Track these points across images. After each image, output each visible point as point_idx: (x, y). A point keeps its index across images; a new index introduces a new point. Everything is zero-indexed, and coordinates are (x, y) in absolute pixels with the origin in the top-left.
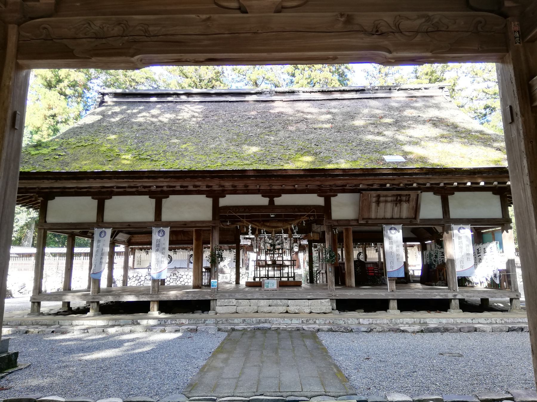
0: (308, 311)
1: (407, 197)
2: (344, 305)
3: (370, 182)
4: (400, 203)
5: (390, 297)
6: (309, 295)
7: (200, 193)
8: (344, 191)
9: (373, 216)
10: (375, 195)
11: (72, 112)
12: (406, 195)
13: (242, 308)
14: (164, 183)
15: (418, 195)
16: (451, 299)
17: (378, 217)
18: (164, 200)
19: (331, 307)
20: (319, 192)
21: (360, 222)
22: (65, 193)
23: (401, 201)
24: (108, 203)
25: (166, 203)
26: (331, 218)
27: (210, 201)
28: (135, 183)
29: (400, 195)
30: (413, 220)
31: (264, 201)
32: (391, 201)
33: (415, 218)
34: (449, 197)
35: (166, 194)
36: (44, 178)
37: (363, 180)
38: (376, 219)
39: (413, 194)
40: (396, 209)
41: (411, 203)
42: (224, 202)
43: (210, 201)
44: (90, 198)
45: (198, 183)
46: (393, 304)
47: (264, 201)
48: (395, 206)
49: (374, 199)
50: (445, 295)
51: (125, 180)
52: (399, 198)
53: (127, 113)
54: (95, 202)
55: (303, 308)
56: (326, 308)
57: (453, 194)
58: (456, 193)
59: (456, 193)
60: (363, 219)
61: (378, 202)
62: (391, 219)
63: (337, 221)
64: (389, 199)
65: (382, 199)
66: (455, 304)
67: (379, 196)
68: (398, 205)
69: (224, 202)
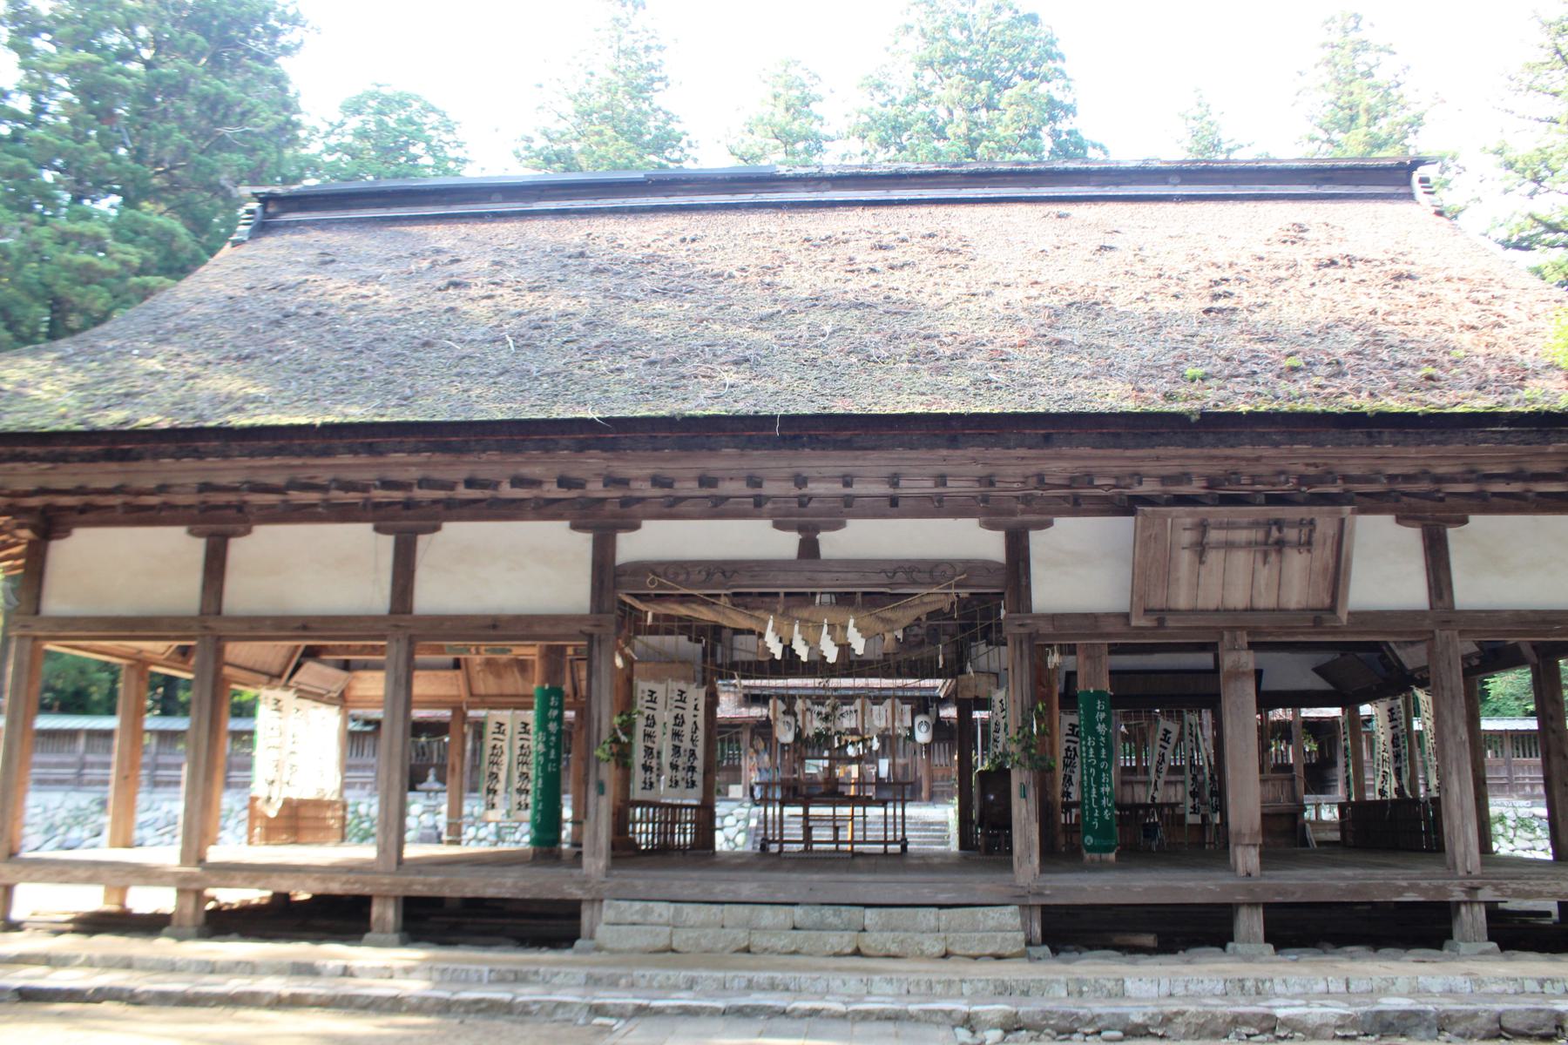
0: (938, 949)
1: (1305, 531)
2: (1067, 931)
3: (1172, 468)
4: (1280, 552)
5: (1239, 898)
6: (943, 891)
7: (545, 510)
8: (1077, 506)
9: (1182, 601)
10: (1188, 521)
12: (1301, 523)
13: (693, 934)
15: (1342, 521)
16: (1458, 904)
17: (1201, 604)
18: (423, 541)
19: (1021, 936)
20: (985, 508)
21: (1134, 623)
22: (95, 513)
23: (1280, 545)
24: (238, 549)
26: (1029, 609)
28: (312, 472)
29: (1279, 524)
30: (1326, 616)
31: (786, 544)
32: (1249, 545)
33: (1332, 609)
34: (1452, 533)
35: (51, 524)
37: (1143, 459)
38: (1193, 611)
39: (1324, 520)
40: (1264, 573)
41: (1317, 552)
42: (632, 546)
44: (366, 529)
45: (669, 469)
46: (1250, 923)
47: (786, 544)
48: (1259, 564)
49: (1187, 537)
50: (1438, 889)
51: (277, 460)
52: (1275, 533)
54: (198, 546)
55: (918, 937)
56: (1005, 940)
57: (1465, 521)
58: (1472, 518)
59: (1472, 518)
60: (1147, 611)
61: (1201, 549)
62: (1246, 610)
63: (1054, 618)
64: (1242, 536)
65: (1214, 535)
66: (1473, 919)
67: (1203, 527)
68: (1273, 557)
69: (632, 546)
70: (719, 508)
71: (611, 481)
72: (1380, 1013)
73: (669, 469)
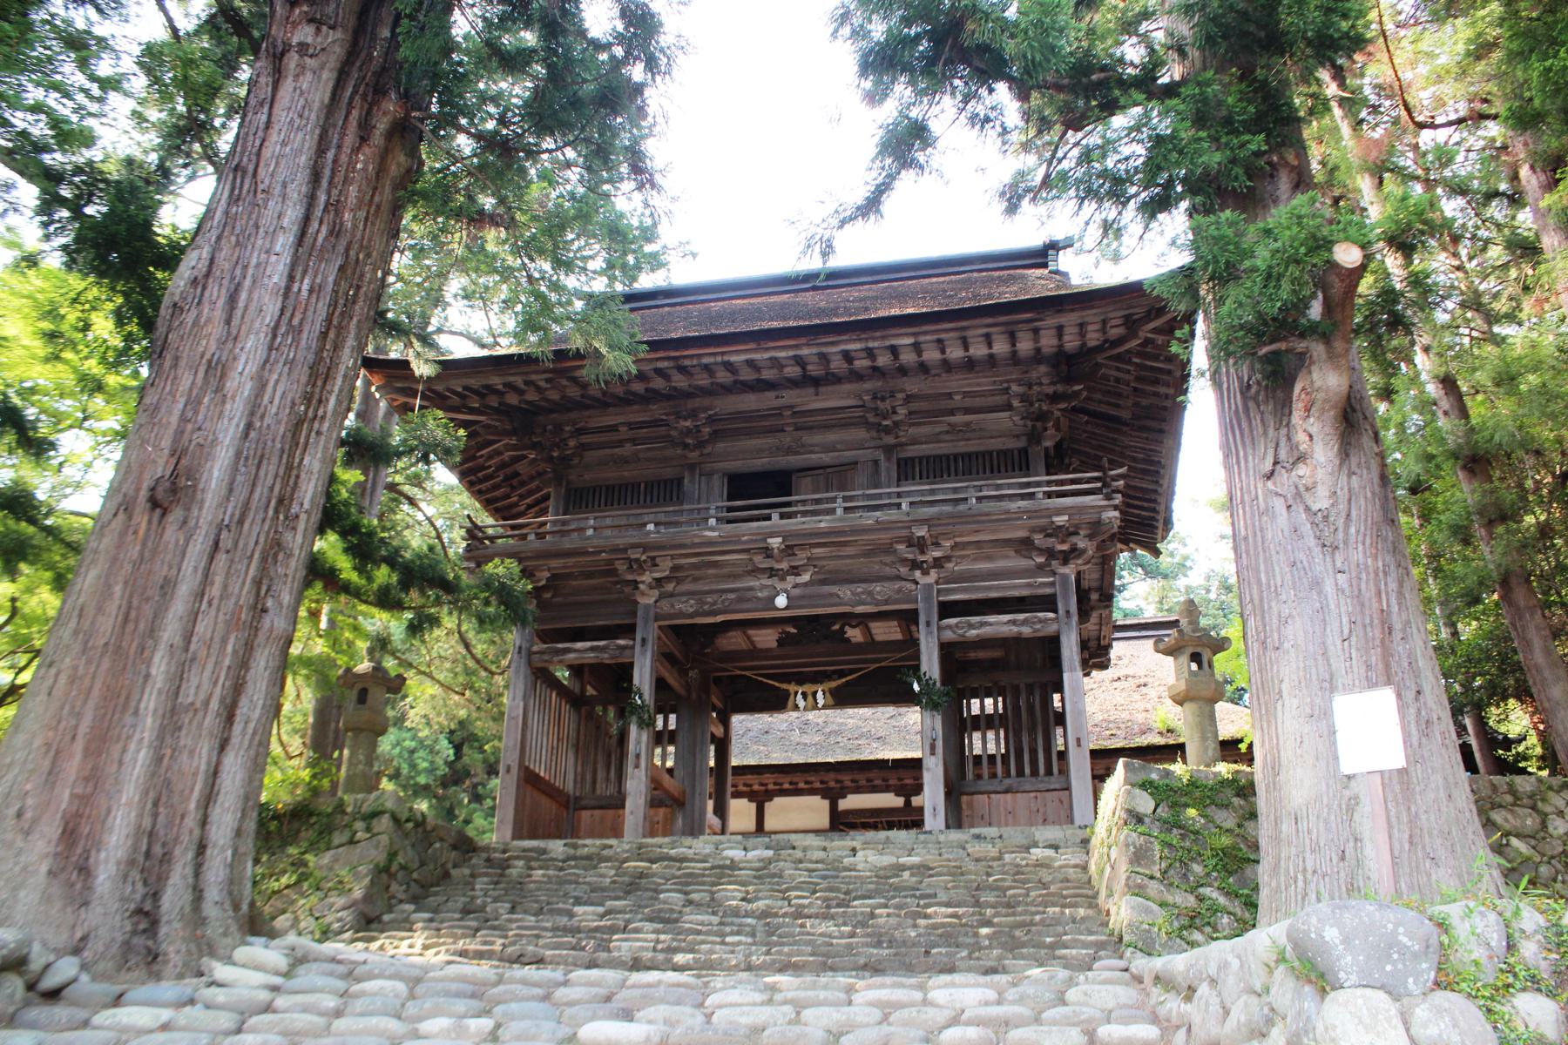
11: (41, 125)
14: (769, 779)
18: (767, 805)
25: (769, 807)
27: (826, 803)
31: (899, 802)
35: (769, 795)
36: (1021, 600)
43: (826, 803)
44: (745, 801)
45: (840, 777)
47: (899, 802)
53: (1313, 296)
70: (874, 789)
71: (837, 781)
72: (1186, 377)
73: (840, 777)
